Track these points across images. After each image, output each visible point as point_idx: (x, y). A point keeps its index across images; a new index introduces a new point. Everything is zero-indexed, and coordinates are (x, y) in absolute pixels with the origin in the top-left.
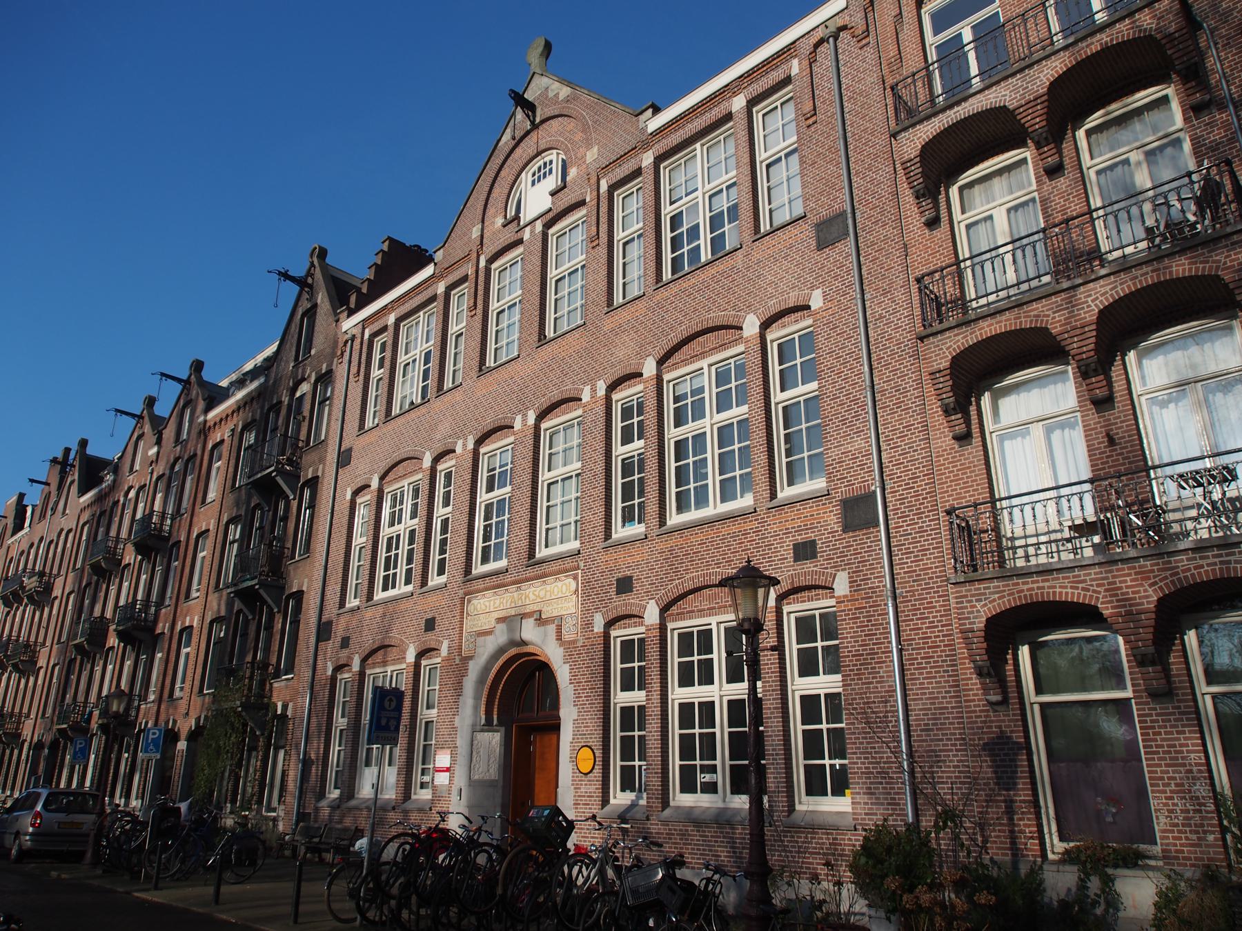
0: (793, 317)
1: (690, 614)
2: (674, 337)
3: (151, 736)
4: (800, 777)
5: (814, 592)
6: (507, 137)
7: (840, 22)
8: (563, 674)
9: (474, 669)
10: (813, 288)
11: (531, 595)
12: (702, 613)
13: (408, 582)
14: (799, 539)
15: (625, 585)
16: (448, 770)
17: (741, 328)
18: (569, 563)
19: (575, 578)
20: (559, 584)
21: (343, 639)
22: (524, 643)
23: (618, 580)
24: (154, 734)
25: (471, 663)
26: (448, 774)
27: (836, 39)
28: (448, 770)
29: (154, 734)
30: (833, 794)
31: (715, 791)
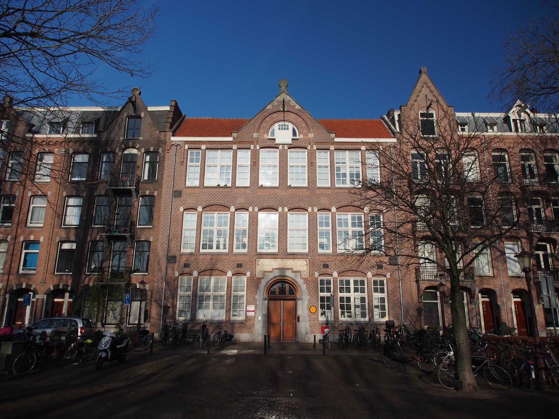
0: (192, 210)
1: (346, 276)
2: (297, 206)
3: (127, 297)
4: (340, 313)
5: (380, 276)
6: (269, 107)
7: (180, 143)
8: (304, 287)
9: (263, 282)
10: (250, 206)
11: (288, 263)
12: (349, 276)
13: (225, 248)
14: (324, 263)
15: (326, 266)
16: (253, 311)
17: (230, 209)
18: (304, 257)
19: (306, 261)
20: (300, 262)
21: (328, 265)
22: (285, 276)
23: (323, 264)
24: (128, 296)
25: (262, 280)
26: (254, 312)
27: (177, 146)
28: (253, 311)
29: (128, 296)
30: (381, 318)
31: (351, 317)
